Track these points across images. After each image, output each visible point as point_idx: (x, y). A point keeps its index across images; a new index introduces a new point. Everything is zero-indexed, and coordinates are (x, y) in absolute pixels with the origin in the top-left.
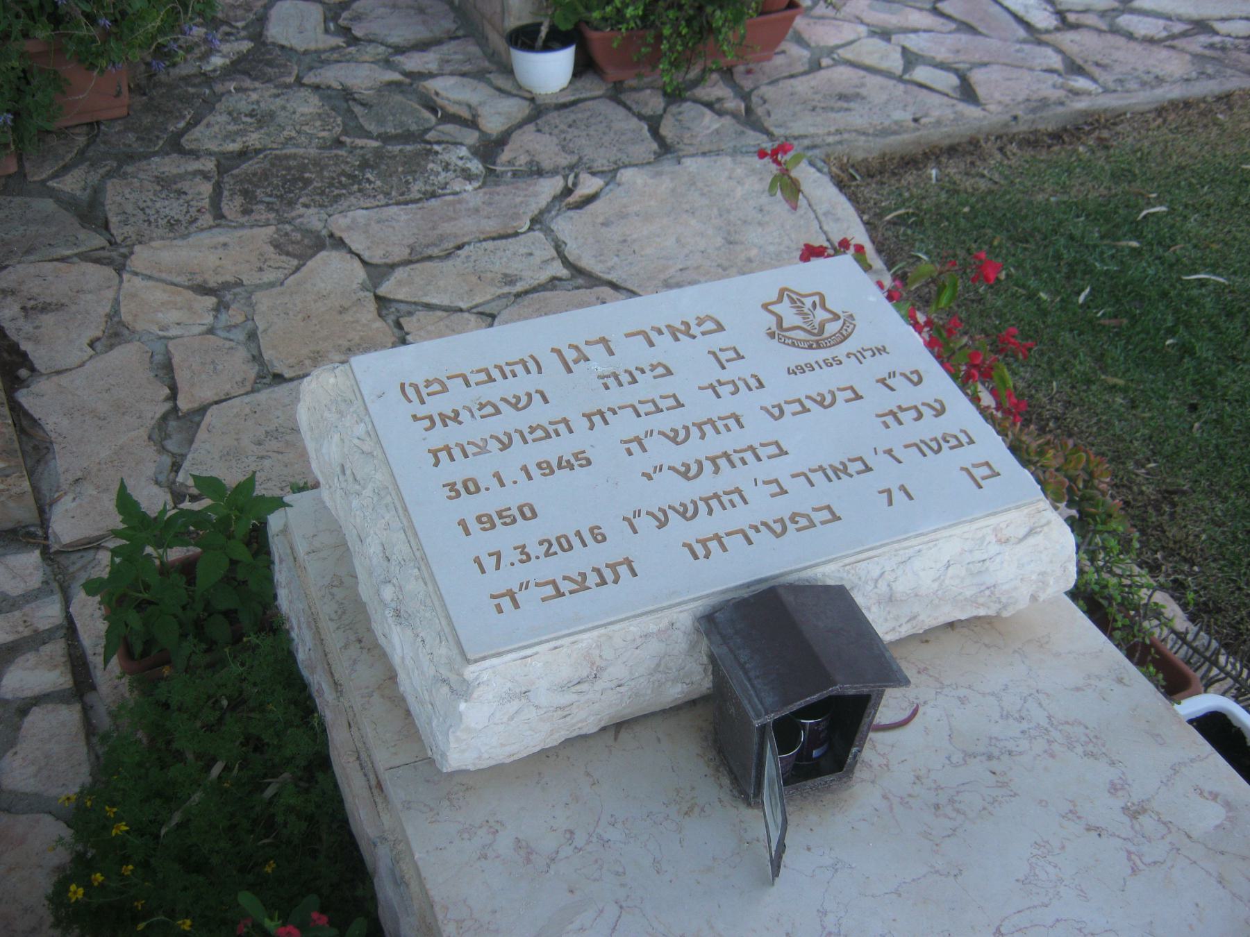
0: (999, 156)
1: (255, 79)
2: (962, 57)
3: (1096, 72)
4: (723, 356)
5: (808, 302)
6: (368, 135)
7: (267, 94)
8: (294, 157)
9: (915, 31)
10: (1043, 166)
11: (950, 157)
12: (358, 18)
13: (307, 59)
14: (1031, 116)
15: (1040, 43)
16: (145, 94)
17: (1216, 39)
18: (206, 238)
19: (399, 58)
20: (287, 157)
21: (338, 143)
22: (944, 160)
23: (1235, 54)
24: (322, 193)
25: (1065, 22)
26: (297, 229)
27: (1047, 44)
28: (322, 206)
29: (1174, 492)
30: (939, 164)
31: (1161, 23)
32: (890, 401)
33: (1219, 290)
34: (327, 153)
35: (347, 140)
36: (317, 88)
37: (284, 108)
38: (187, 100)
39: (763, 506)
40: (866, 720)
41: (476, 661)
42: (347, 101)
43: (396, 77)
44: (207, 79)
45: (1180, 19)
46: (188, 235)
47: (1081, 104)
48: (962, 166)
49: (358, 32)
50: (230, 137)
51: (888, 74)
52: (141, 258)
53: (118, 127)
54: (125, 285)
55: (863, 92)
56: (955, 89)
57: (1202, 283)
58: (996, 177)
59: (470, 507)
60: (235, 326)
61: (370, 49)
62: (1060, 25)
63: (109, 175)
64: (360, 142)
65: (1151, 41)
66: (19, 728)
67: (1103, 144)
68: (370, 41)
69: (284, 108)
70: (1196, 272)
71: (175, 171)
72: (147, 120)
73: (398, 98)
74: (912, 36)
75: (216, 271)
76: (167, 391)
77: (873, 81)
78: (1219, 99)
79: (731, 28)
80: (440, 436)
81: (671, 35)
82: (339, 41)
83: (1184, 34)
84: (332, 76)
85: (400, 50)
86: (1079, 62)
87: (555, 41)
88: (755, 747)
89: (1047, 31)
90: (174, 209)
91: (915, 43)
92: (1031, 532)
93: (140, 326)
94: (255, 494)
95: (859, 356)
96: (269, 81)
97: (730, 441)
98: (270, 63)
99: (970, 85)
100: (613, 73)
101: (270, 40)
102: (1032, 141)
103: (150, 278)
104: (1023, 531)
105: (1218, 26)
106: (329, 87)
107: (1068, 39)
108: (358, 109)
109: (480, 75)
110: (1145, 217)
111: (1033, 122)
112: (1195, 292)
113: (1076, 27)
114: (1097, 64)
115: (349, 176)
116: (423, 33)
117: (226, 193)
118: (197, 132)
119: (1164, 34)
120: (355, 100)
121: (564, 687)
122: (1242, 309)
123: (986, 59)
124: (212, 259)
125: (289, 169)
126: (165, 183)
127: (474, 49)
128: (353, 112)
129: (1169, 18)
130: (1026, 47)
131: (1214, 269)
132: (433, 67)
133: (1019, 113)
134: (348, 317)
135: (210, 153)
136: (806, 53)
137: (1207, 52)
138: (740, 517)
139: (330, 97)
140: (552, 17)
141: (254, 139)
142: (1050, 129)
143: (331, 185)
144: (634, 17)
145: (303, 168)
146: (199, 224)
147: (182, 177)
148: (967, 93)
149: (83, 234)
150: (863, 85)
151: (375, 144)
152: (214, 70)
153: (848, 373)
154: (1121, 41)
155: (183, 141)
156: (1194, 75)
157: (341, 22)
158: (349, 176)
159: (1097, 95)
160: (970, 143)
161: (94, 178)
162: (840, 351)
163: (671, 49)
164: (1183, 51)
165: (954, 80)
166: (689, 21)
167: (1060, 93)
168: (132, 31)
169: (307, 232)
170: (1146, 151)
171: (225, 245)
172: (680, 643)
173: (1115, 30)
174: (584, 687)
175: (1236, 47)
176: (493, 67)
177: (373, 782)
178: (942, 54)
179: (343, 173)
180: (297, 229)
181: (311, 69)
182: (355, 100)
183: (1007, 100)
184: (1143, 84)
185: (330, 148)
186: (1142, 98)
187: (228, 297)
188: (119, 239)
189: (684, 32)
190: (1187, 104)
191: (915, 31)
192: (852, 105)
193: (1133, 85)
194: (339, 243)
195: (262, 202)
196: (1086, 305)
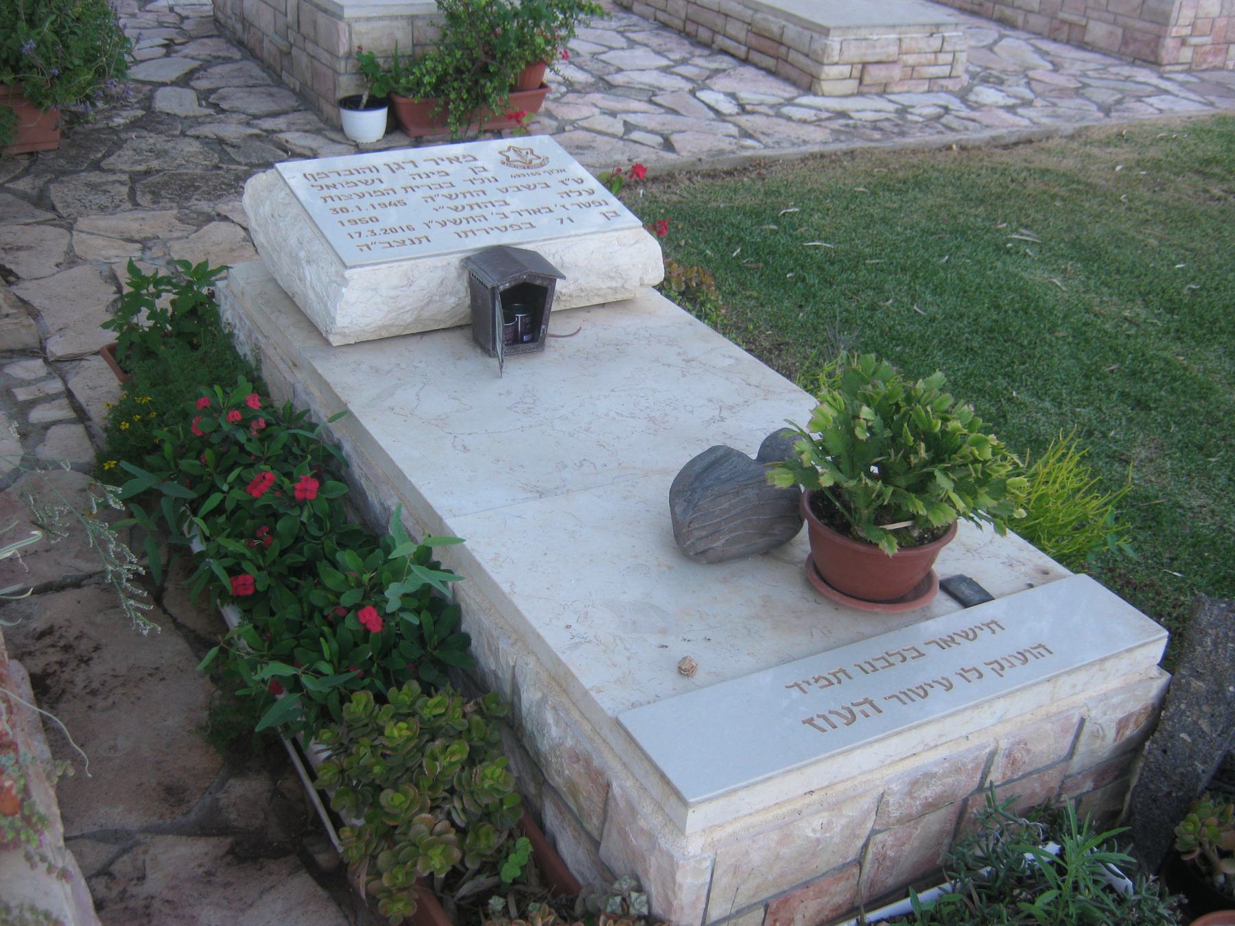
0: (687, 182)
1: (151, 131)
2: (666, 127)
3: (762, 137)
4: (477, 170)
5: (524, 152)
6: (239, 163)
7: (161, 140)
8: (186, 174)
9: (635, 112)
10: (717, 188)
11: (653, 183)
12: (224, 98)
13: (188, 122)
14: (712, 159)
15: (724, 121)
16: (68, 138)
17: (851, 122)
18: (129, 215)
19: (255, 122)
20: (181, 174)
21: (217, 167)
22: (649, 184)
23: (862, 130)
24: (209, 193)
25: (743, 109)
26: (192, 212)
27: (729, 122)
28: (210, 200)
29: (782, 344)
30: (645, 187)
31: (813, 112)
32: (565, 188)
33: (827, 252)
34: (210, 173)
35: (224, 166)
36: (197, 137)
37: (174, 148)
38: (103, 142)
39: (495, 221)
40: (546, 312)
41: (351, 268)
42: (220, 144)
43: (256, 131)
44: (113, 130)
45: (827, 110)
46: (115, 214)
47: (749, 153)
48: (662, 188)
49: (224, 105)
50: (139, 162)
51: (613, 136)
52: (83, 223)
53: (52, 155)
54: (75, 237)
55: (594, 145)
56: (660, 144)
57: (816, 247)
58: (685, 194)
59: (344, 217)
60: (158, 258)
61: (235, 116)
62: (740, 111)
63: (50, 181)
64: (233, 167)
65: (804, 122)
66: (44, 435)
67: (761, 177)
68: (234, 112)
69: (174, 148)
70: (813, 241)
71: (99, 180)
72: (73, 152)
73: (258, 143)
74: (633, 115)
75: (139, 231)
76: (115, 289)
77: (599, 138)
78: (845, 153)
79: (497, 95)
80: (326, 193)
81: (456, 100)
82: (212, 111)
83: (829, 119)
84: (208, 130)
85: (256, 117)
86: (751, 132)
87: (373, 104)
88: (491, 312)
89: (731, 115)
90: (103, 200)
91: (631, 118)
92: (637, 242)
93: (89, 258)
94: (209, 269)
95: (551, 172)
96: (161, 133)
97: (482, 199)
98: (161, 123)
99: (670, 142)
100: (414, 131)
101: (158, 110)
102: (712, 175)
103: (92, 234)
104: (632, 242)
105: (853, 114)
106: (206, 137)
107: (744, 120)
108: (229, 149)
109: (318, 132)
110: (784, 214)
111: (713, 162)
112: (811, 252)
113: (752, 113)
114: (763, 133)
115: (227, 185)
116: (274, 107)
117: (138, 193)
118: (111, 159)
119: (815, 118)
120: (227, 144)
121: (395, 288)
122: (841, 261)
123: (683, 129)
124: (135, 226)
125: (183, 181)
126: (93, 187)
127: (311, 117)
128: (226, 151)
129: (820, 110)
130: (713, 123)
131: (826, 240)
132: (283, 127)
133: (703, 157)
134: (236, 254)
135: (123, 172)
136: (554, 124)
137: (843, 129)
138: (484, 224)
139: (208, 143)
140: (371, 89)
141: (155, 164)
142: (725, 169)
143: (215, 189)
144: (430, 83)
145: (193, 180)
146: (122, 207)
147: (104, 184)
148: (668, 145)
149: (37, 212)
150: (594, 141)
151: (245, 168)
152: (119, 126)
153: (545, 178)
154: (783, 121)
155: (101, 164)
156: (831, 140)
157: (210, 100)
158: (227, 185)
159: (760, 149)
160: (668, 175)
161: (40, 182)
162: (541, 170)
163: (456, 108)
164: (826, 127)
165: (660, 140)
166: (468, 91)
167: (734, 147)
168: (69, 82)
169: (200, 213)
170: (790, 180)
171: (143, 219)
172: (453, 273)
173: (779, 115)
174: (405, 288)
175: (864, 127)
176: (328, 128)
177: (290, 364)
178: (652, 125)
179: (223, 183)
180: (192, 212)
181: (191, 127)
182: (227, 144)
183: (696, 150)
184: (793, 144)
185: (212, 170)
186: (789, 151)
187: (150, 244)
188: (65, 215)
189: (465, 97)
190: (822, 156)
191: (635, 112)
192: (586, 152)
193: (785, 144)
194: (225, 218)
195: (165, 198)
196: (737, 257)
